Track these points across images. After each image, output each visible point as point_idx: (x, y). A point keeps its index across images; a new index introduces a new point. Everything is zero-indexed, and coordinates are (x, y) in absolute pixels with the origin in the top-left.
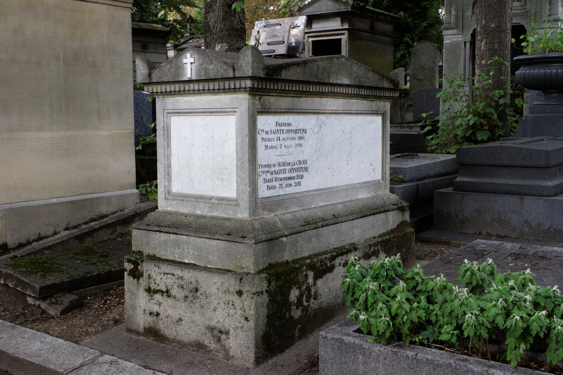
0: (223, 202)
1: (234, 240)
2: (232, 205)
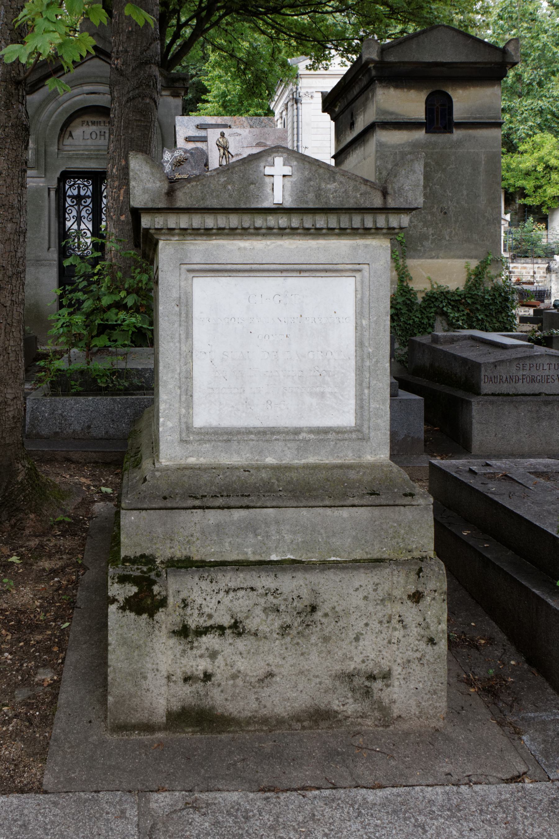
0: (330, 436)
1: (392, 503)
2: (350, 440)
